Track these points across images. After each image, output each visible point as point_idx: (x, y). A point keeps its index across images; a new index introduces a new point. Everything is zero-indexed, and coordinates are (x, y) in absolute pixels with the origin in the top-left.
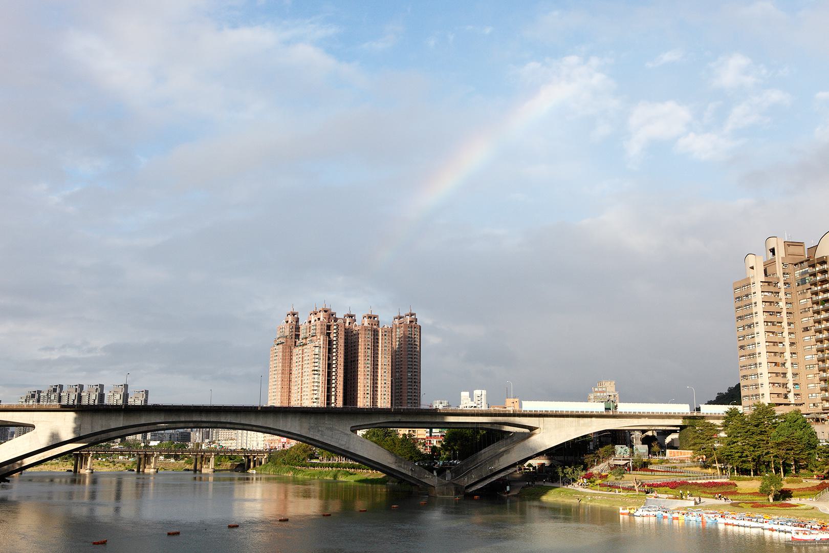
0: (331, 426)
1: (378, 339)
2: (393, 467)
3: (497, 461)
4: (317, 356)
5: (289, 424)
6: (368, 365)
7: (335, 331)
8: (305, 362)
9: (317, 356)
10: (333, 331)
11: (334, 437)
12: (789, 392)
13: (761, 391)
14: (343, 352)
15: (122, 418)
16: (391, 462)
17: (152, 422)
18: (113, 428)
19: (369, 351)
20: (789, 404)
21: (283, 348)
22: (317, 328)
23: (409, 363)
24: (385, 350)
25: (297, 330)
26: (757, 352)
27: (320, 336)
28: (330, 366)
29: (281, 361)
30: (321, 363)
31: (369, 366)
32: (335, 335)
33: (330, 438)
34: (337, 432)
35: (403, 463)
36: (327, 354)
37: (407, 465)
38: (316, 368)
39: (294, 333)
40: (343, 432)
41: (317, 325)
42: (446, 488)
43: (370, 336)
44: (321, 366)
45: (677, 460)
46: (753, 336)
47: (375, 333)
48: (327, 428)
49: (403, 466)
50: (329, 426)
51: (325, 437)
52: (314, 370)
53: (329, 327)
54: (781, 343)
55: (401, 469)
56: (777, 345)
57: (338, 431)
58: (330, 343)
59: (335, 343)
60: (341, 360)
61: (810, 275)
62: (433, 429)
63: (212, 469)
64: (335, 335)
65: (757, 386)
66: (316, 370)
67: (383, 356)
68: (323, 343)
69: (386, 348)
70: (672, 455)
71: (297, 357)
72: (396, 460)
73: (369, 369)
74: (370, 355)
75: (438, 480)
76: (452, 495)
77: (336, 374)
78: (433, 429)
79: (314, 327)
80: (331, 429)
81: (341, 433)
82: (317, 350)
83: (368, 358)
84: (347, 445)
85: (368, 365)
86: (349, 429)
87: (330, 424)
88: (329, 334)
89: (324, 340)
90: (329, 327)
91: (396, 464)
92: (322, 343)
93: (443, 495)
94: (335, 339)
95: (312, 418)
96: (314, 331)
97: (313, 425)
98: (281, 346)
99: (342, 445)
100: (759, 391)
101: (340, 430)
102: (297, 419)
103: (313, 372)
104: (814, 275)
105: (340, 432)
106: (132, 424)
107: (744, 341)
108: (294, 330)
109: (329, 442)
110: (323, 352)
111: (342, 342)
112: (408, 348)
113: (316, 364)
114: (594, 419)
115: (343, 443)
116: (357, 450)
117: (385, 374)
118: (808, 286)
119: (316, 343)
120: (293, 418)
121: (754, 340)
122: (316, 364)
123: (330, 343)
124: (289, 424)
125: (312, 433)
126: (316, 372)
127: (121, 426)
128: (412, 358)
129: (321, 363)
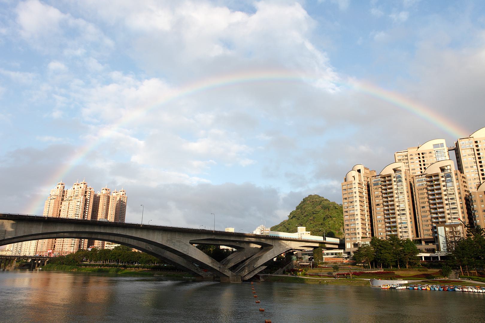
0: (179, 240)
1: (109, 201)
2: (210, 265)
3: (256, 263)
4: (78, 207)
5: (156, 237)
6: (103, 214)
7: (89, 194)
8: (70, 209)
9: (78, 207)
10: (88, 194)
11: (181, 246)
12: (367, 232)
13: (357, 231)
14: (92, 206)
15: (41, 227)
16: (209, 262)
17: (65, 231)
18: (33, 234)
19: (105, 207)
20: (366, 238)
21: (55, 201)
22: (80, 192)
23: (120, 215)
24: (112, 207)
25: (63, 193)
26: (356, 213)
27: (81, 196)
28: (84, 212)
29: (52, 208)
30: (80, 210)
31: (104, 214)
32: (89, 196)
33: (178, 247)
35: (215, 263)
36: (84, 206)
37: (217, 264)
38: (77, 213)
39: (62, 194)
40: (185, 244)
41: (80, 190)
42: (236, 278)
43: (106, 199)
44: (80, 212)
45: (332, 262)
46: (353, 207)
47: (109, 198)
48: (177, 241)
49: (215, 265)
50: (178, 240)
51: (176, 246)
52: (76, 214)
53: (86, 192)
54: (364, 210)
55: (214, 266)
56: (363, 211)
58: (86, 200)
59: (88, 200)
60: (91, 210)
61: (381, 182)
62: (220, 246)
63: (14, 267)
64: (89, 196)
65: (355, 229)
67: (111, 210)
68: (83, 200)
69: (113, 206)
70: (327, 260)
71: (65, 206)
72: (212, 261)
73: (104, 216)
74: (105, 208)
75: (231, 273)
76: (240, 282)
77: (87, 217)
78: (220, 246)
79: (78, 191)
80: (179, 242)
81: (184, 244)
82: (79, 204)
83: (104, 210)
84: (187, 252)
85: (103, 214)
86: (188, 242)
87: (178, 239)
88: (85, 196)
89: (83, 198)
90: (86, 192)
91: (212, 264)
92: (82, 200)
93: (234, 281)
94: (89, 198)
95: (169, 234)
96: (78, 194)
97: (169, 238)
98: (53, 200)
99: (185, 252)
100: (356, 232)
101: (184, 242)
102: (161, 234)
103: (75, 215)
104: (385, 182)
105: (184, 244)
106: (49, 231)
107: (347, 209)
108: (62, 192)
109: (177, 250)
110: (82, 205)
111: (92, 200)
112: (121, 207)
113: (77, 211)
114: (292, 242)
115: (185, 250)
116: (192, 255)
117: (111, 219)
118: (380, 186)
119: (79, 200)
120: (158, 234)
121: (354, 208)
122: (77, 211)
123: (86, 200)
124: (156, 237)
125: (169, 243)
126: (77, 215)
127: (41, 233)
128: (122, 212)
129: (80, 210)
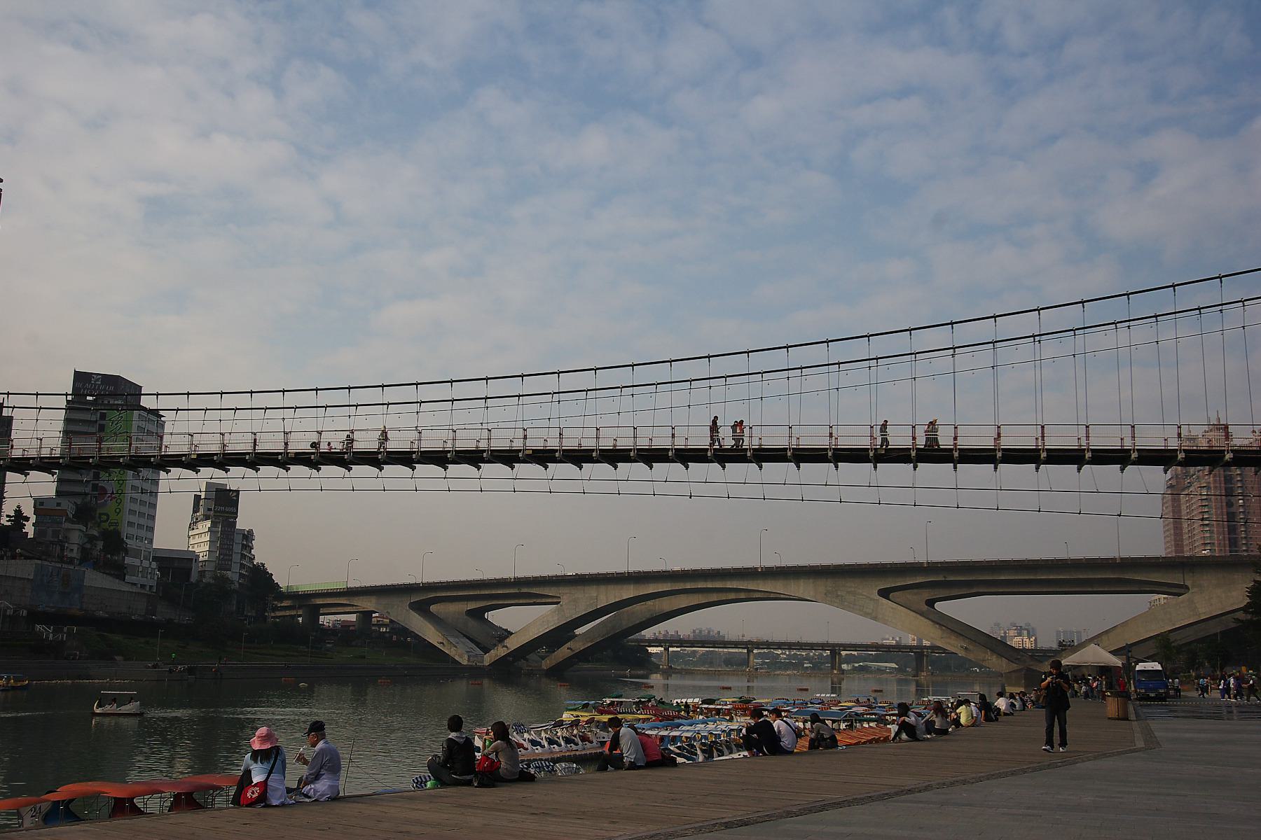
34: (861, 597)
57: (863, 595)
66: (1207, 525)
101: (865, 593)
